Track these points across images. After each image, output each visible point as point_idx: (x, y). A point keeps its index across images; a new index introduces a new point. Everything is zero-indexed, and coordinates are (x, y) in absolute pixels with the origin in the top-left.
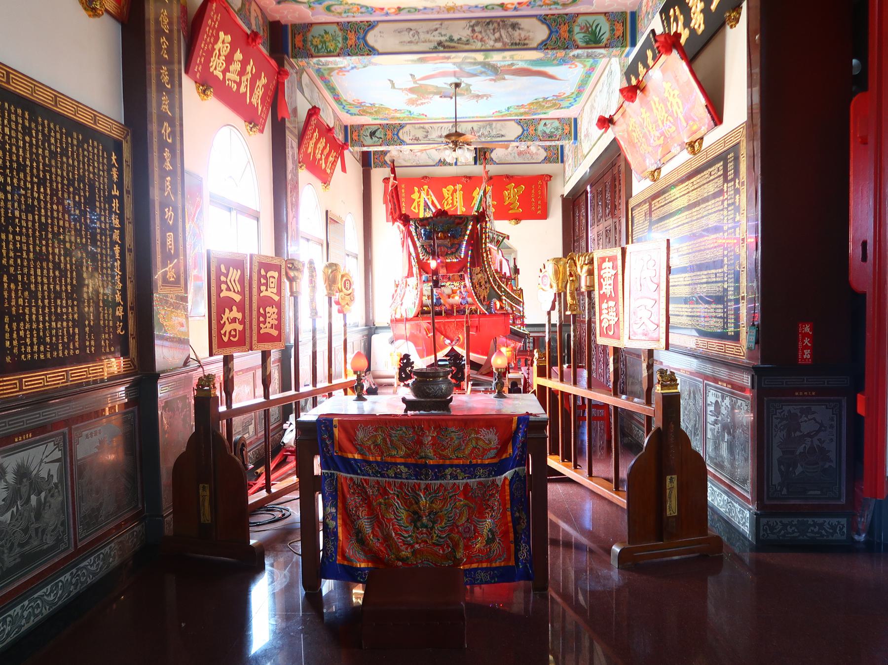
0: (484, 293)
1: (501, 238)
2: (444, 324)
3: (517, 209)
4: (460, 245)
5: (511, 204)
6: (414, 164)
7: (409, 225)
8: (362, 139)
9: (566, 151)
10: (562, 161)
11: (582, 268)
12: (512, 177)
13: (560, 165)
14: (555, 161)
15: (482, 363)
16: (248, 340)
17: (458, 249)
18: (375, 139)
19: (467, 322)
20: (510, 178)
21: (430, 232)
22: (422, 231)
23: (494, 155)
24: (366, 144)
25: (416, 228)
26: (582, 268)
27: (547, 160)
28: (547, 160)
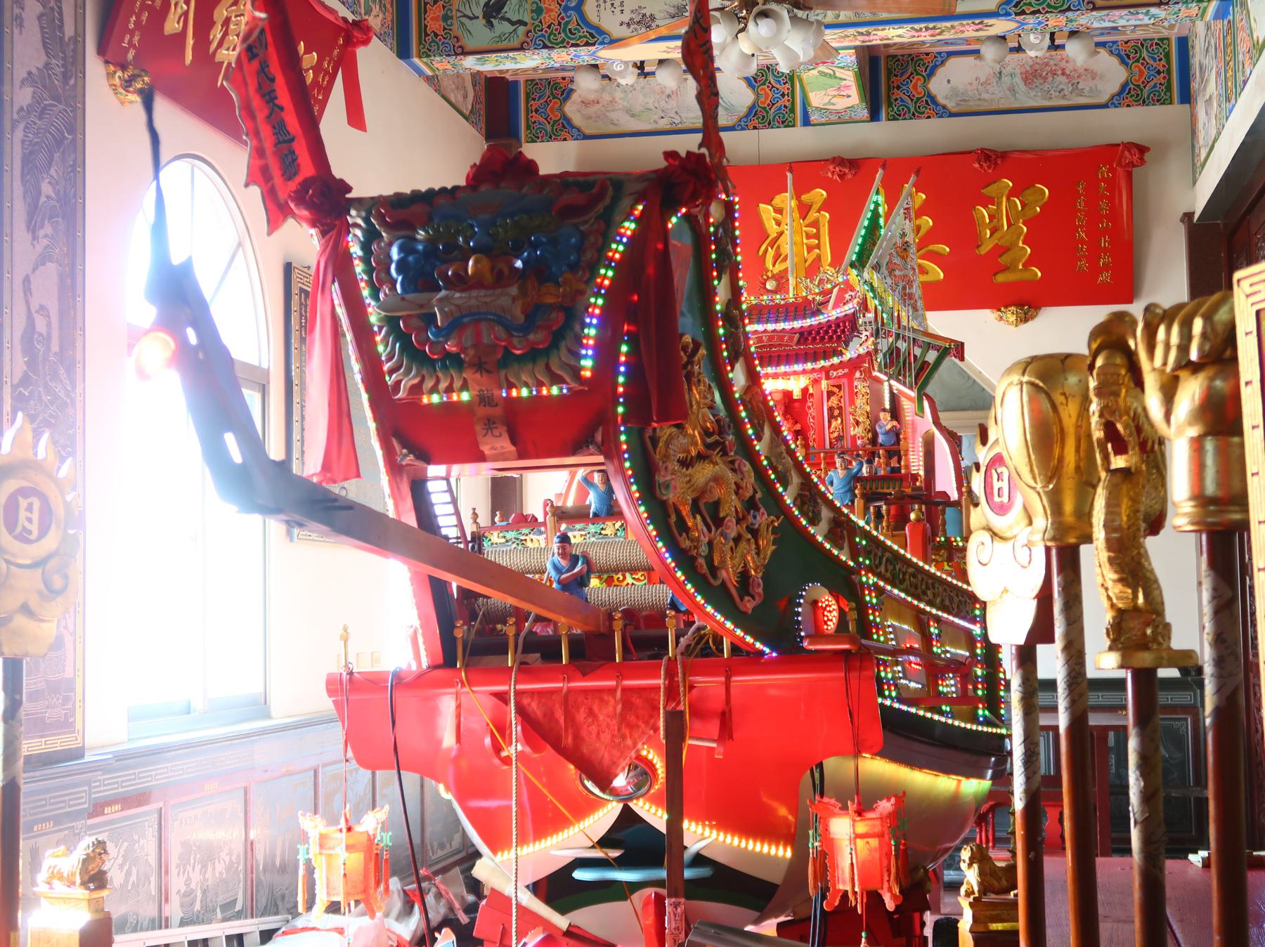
0: (742, 559)
1: (932, 356)
2: (569, 701)
3: (1023, 268)
4: (572, 314)
5: (1000, 250)
6: (663, 124)
7: (347, 228)
8: (456, 30)
9: (1198, 56)
10: (1187, 97)
11: (1169, 391)
12: (1004, 155)
13: (1176, 110)
14: (1162, 99)
15: (776, 877)
16: (1059, 630)
17: (564, 331)
18: (502, 27)
19: (672, 693)
20: (993, 160)
21: (431, 252)
22: (395, 253)
23: (938, 86)
24: (470, 44)
25: (371, 236)
26: (1169, 391)
27: (1128, 95)
28: (1128, 95)
